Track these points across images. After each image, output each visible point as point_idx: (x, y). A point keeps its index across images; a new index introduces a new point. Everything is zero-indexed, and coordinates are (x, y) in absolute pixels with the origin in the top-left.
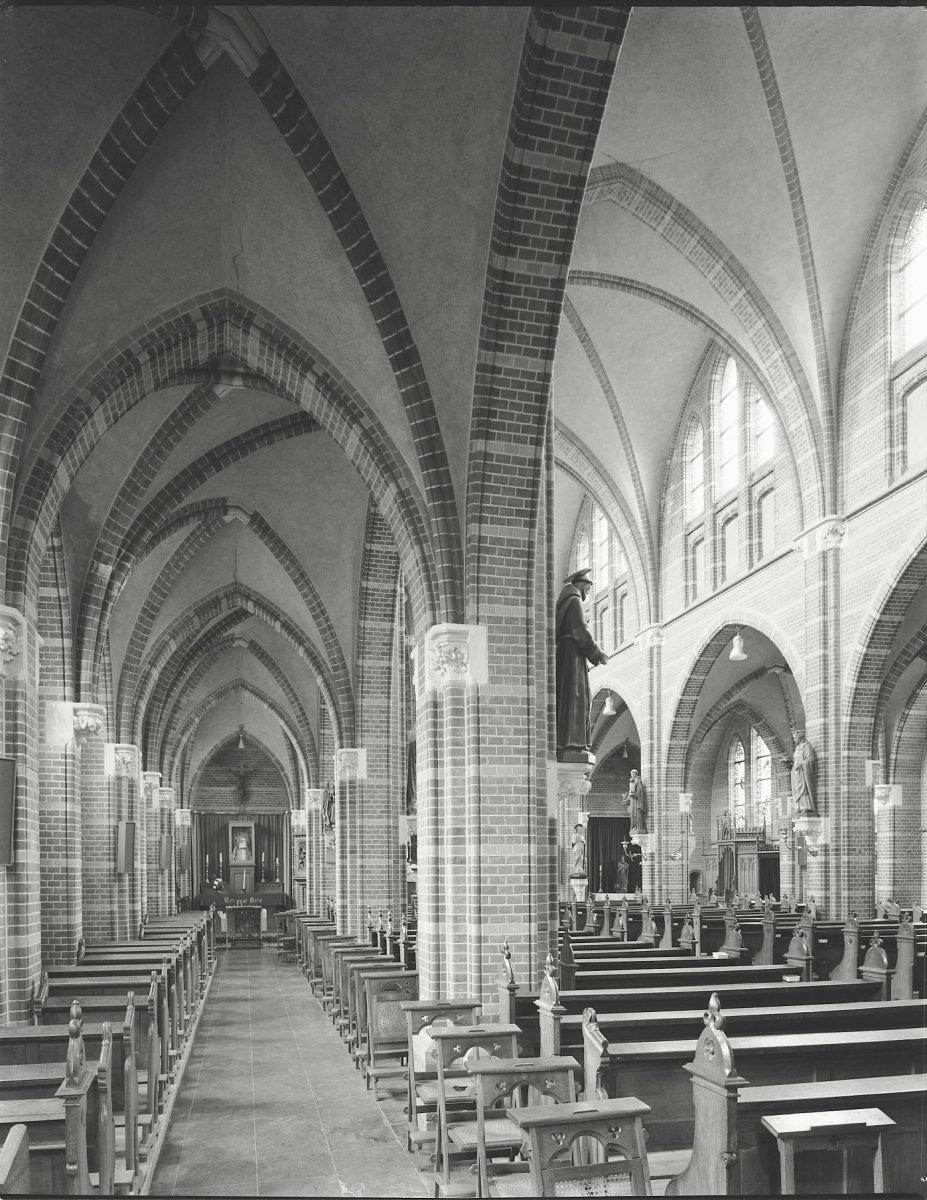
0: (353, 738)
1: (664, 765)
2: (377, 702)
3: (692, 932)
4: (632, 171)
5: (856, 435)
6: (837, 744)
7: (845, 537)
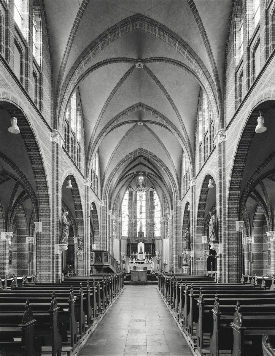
0: (38, 218)
1: (196, 227)
2: (45, 206)
3: (263, 284)
4: (143, 15)
5: (229, 96)
6: (224, 215)
7: (226, 136)
